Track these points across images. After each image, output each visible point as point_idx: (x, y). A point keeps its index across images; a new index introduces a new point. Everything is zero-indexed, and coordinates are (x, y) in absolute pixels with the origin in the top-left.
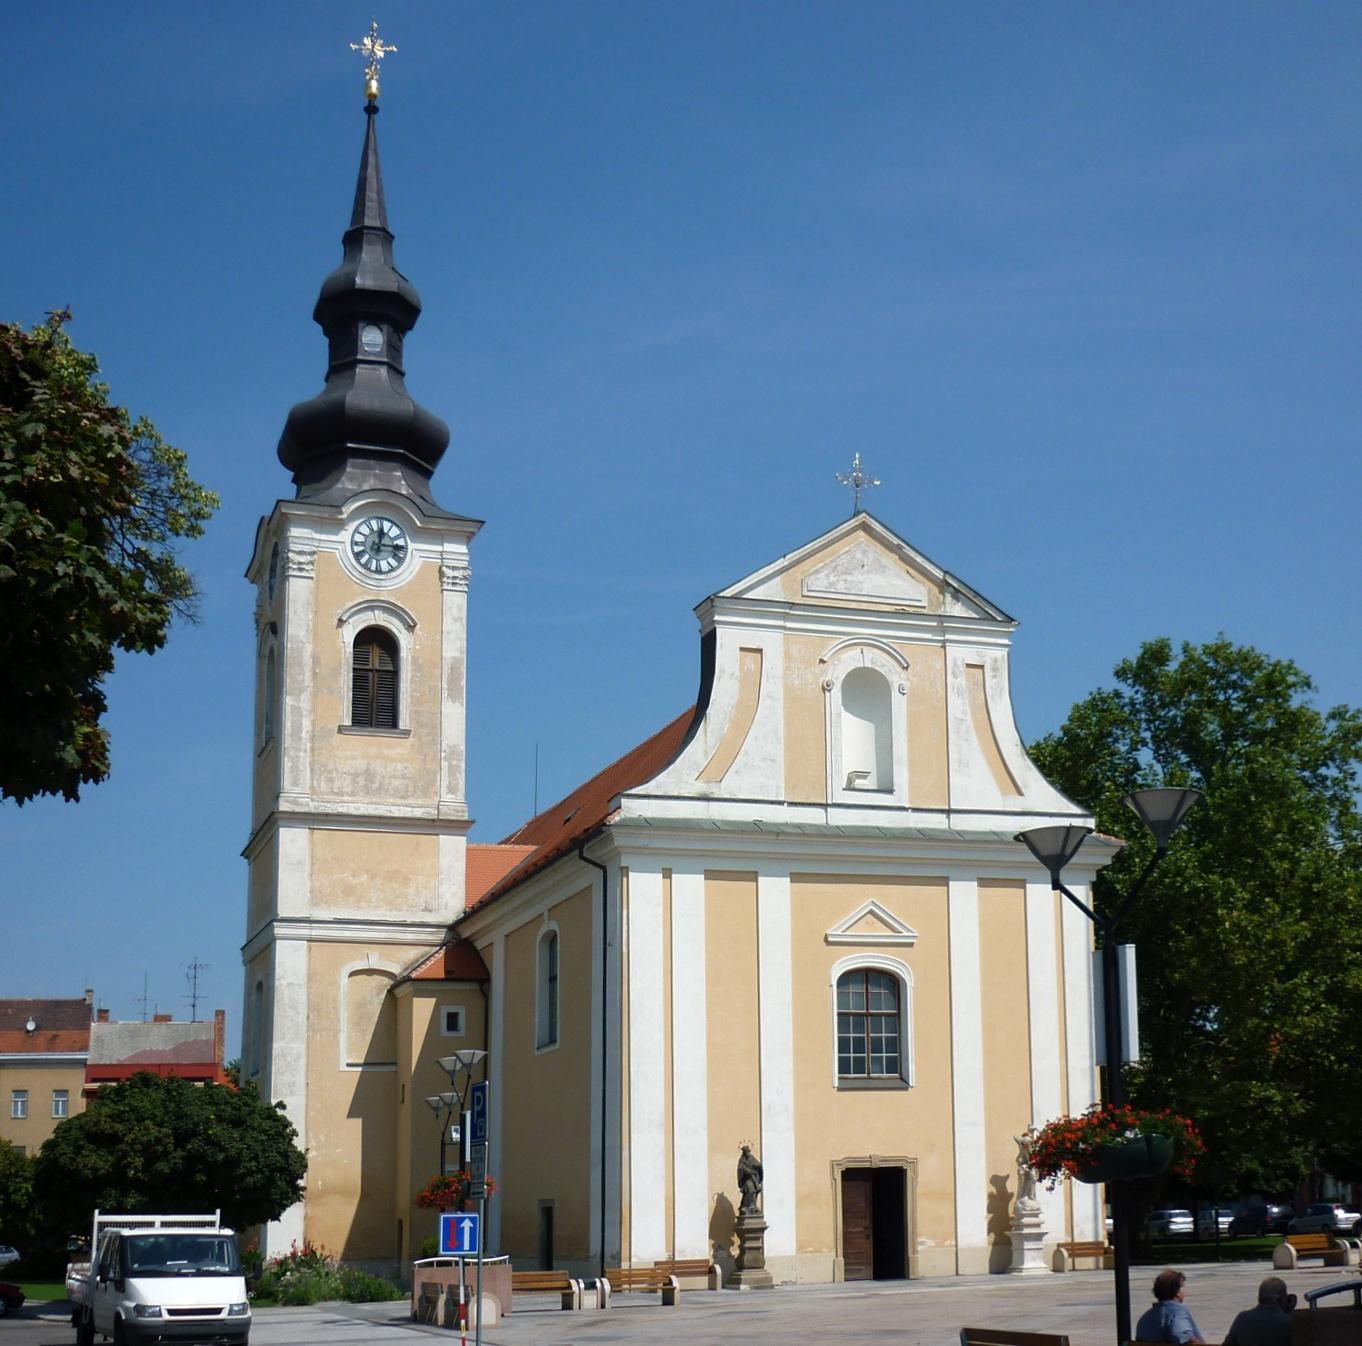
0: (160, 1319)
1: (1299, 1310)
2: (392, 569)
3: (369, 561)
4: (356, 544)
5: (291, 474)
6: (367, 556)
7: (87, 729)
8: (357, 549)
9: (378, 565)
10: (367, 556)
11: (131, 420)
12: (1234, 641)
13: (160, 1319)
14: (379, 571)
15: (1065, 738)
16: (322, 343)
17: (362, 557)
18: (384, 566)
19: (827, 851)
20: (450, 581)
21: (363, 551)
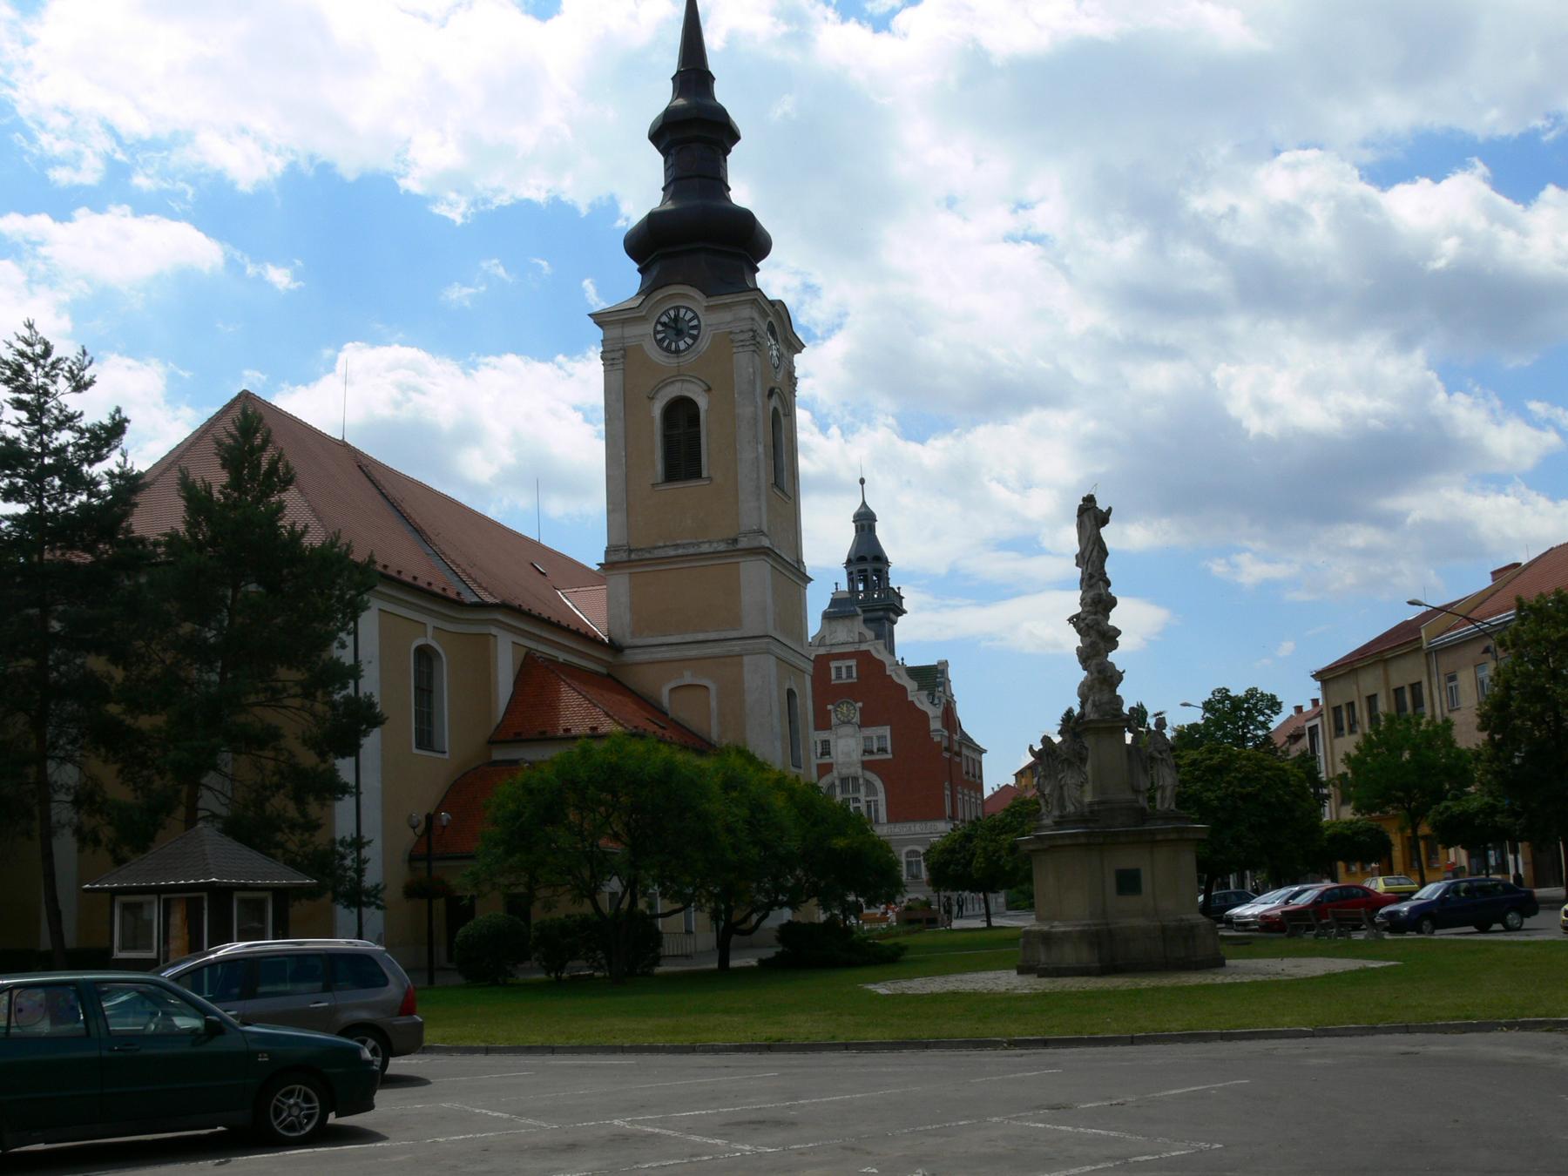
0: (272, 1117)
1: (330, 1125)
2: (689, 346)
3: (670, 344)
4: (659, 332)
5: (636, 266)
6: (667, 341)
7: (334, 600)
8: (695, 332)
9: (677, 346)
10: (667, 341)
11: (68, 356)
12: (76, 409)
13: (272, 1117)
14: (678, 351)
15: (59, 544)
16: (723, 94)
17: (694, 335)
18: (682, 345)
19: (537, 631)
20: (616, 362)
21: (664, 337)
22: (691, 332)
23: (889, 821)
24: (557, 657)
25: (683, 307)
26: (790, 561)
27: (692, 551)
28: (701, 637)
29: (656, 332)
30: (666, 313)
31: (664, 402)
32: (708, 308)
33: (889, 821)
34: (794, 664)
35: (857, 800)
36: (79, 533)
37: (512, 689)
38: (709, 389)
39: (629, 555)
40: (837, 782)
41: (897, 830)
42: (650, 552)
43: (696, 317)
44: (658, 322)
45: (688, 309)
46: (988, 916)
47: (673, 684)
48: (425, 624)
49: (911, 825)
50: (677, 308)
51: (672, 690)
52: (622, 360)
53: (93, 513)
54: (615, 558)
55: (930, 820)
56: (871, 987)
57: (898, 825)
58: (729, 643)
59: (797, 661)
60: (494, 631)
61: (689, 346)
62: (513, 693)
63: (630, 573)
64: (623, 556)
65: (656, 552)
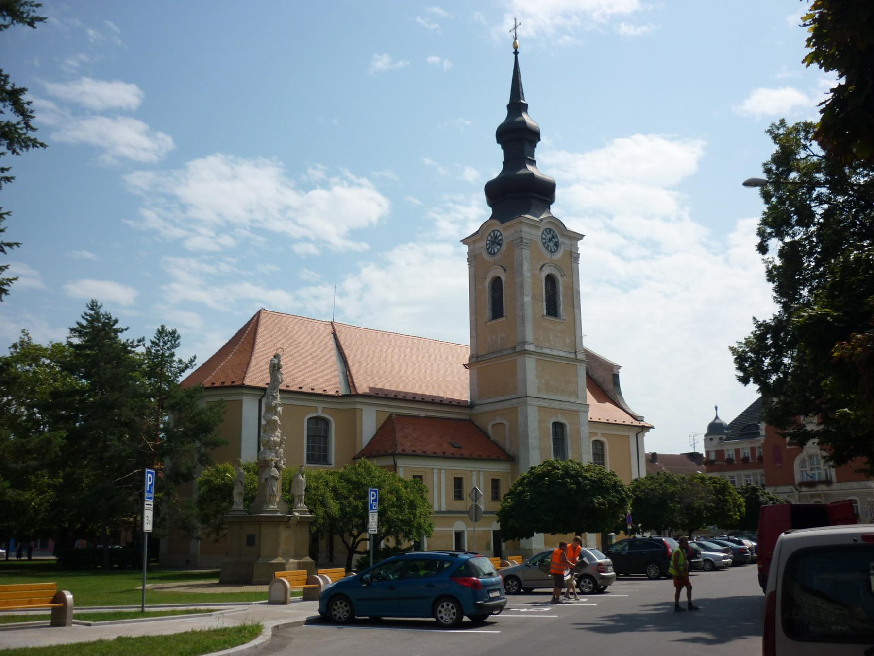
2: (499, 250)
9: (494, 251)
22: (489, 246)
23: (838, 481)
24: (420, 415)
25: (496, 230)
26: (562, 354)
27: (499, 355)
28: (503, 398)
29: (487, 245)
30: (490, 234)
31: (491, 278)
32: (504, 229)
33: (838, 481)
34: (550, 407)
35: (818, 469)
36: (24, 399)
37: (375, 433)
38: (505, 270)
39: (477, 359)
40: (806, 458)
41: (843, 487)
42: (484, 357)
43: (501, 234)
44: (487, 240)
45: (498, 231)
46: (474, 530)
47: (492, 423)
48: (317, 407)
49: (851, 483)
50: (494, 231)
51: (494, 425)
52: (474, 261)
53: (871, 263)
54: (472, 361)
55: (862, 481)
56: (273, 561)
57: (843, 484)
58: (512, 401)
59: (568, 407)
60: (358, 406)
61: (499, 250)
62: (375, 436)
63: (536, 359)
64: (475, 359)
65: (487, 356)
